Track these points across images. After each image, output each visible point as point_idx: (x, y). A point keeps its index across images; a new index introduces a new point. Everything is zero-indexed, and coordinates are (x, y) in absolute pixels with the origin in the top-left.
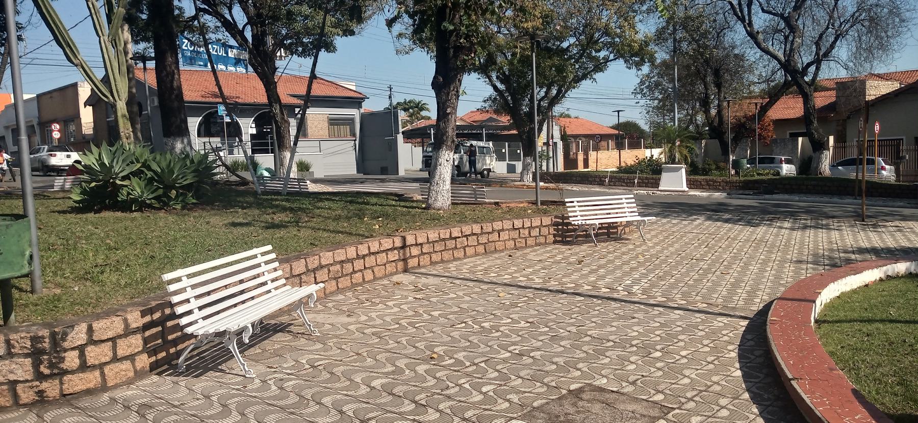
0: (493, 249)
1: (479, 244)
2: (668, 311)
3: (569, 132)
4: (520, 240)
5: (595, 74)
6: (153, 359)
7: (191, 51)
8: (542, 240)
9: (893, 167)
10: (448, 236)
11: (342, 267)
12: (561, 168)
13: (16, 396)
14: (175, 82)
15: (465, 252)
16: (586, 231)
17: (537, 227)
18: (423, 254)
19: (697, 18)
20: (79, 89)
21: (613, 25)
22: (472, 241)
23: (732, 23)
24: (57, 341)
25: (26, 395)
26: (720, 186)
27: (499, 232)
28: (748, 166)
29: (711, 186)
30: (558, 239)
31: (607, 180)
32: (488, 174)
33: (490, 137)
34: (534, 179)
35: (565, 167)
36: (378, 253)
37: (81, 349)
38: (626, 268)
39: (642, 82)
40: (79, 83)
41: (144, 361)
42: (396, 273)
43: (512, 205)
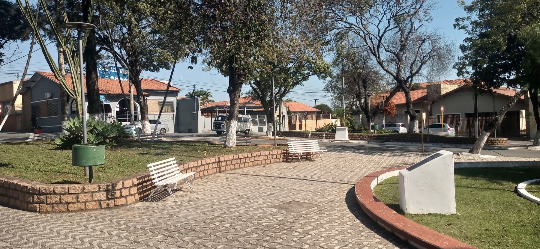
0: (256, 164)
1: (250, 162)
2: (325, 183)
3: (291, 110)
4: (268, 160)
5: (303, 81)
6: (140, 196)
7: (103, 71)
8: (278, 160)
9: (454, 129)
10: (237, 158)
11: (196, 169)
12: (287, 129)
13: (101, 205)
14: (96, 87)
15: (244, 165)
16: (297, 156)
17: (275, 154)
18: (227, 165)
19: (353, 54)
20: (14, 84)
21: (311, 58)
22: (248, 160)
23: (371, 56)
24: (114, 186)
25: (104, 205)
26: (365, 138)
27: (259, 156)
28: (119, 122)
29: (362, 138)
30: (285, 160)
31: (310, 135)
32: (249, 132)
33: (249, 112)
34: (273, 134)
35: (290, 128)
36: (209, 164)
37: (120, 190)
38: (313, 170)
39: (327, 85)
40: (14, 82)
41: (137, 197)
42: (216, 173)
43: (263, 146)
